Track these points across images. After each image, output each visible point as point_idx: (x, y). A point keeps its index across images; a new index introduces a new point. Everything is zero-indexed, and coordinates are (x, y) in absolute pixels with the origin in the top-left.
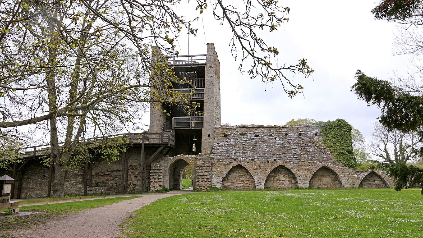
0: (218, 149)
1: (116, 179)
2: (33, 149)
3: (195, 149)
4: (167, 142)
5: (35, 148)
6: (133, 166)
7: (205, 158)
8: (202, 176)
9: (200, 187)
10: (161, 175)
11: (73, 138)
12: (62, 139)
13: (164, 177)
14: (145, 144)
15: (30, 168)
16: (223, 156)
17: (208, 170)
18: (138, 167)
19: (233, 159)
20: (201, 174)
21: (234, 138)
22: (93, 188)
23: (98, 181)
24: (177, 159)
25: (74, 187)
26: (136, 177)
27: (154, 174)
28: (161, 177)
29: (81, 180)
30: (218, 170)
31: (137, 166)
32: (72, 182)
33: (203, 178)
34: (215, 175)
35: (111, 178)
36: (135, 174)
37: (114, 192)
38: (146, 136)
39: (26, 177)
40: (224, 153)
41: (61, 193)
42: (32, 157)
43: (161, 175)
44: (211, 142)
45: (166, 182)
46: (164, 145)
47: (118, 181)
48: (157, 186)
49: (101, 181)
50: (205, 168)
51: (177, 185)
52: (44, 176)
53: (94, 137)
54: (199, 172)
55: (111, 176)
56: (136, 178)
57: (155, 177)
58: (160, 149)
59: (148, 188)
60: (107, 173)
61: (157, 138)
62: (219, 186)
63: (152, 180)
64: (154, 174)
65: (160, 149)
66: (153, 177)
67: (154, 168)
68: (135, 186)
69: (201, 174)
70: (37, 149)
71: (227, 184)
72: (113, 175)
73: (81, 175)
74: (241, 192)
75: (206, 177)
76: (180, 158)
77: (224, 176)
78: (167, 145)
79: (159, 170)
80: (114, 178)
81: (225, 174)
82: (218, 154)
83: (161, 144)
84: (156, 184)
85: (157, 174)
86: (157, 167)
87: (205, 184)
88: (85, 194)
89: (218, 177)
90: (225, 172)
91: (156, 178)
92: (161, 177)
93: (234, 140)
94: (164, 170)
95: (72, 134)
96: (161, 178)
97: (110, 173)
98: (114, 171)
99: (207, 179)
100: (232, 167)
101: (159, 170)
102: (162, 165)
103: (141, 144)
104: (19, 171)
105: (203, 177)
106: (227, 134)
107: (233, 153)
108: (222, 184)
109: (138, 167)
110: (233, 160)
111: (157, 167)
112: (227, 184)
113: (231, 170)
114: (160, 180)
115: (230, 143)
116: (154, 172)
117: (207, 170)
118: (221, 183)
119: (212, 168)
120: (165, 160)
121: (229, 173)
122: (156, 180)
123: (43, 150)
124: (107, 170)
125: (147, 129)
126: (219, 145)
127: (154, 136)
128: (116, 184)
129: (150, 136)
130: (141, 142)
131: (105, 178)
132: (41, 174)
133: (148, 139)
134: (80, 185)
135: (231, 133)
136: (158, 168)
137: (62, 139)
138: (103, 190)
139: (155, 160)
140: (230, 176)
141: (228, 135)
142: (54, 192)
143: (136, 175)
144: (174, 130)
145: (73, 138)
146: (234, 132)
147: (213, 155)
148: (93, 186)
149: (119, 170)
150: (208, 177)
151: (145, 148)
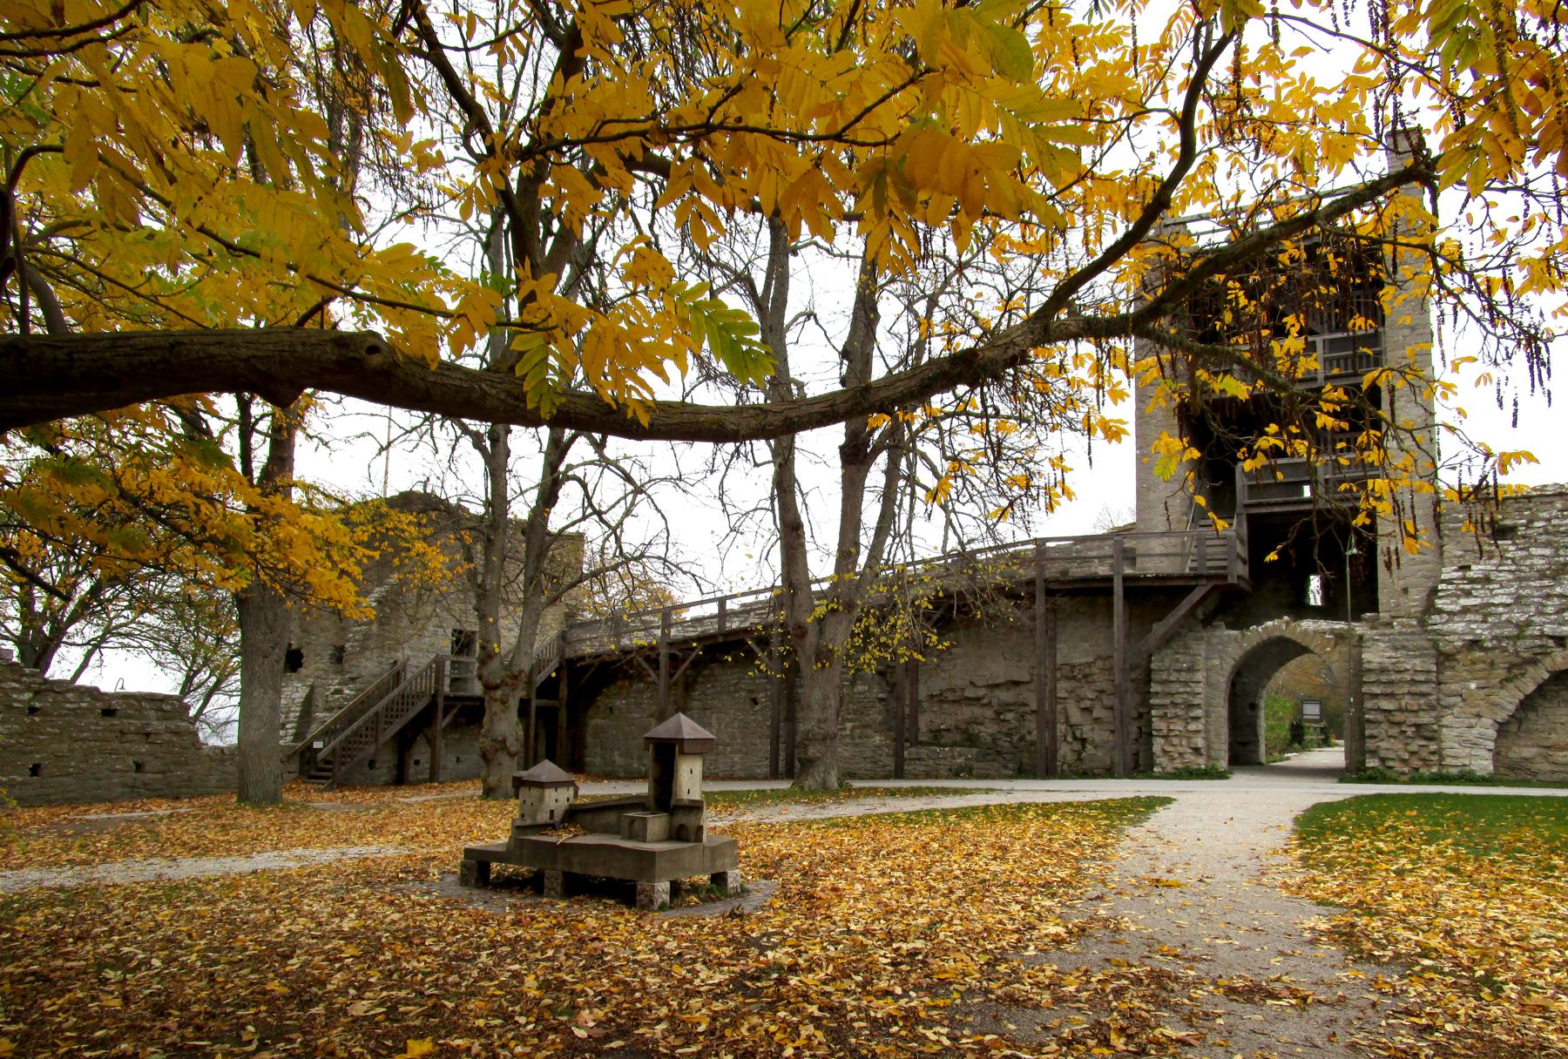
0: (1468, 594)
1: (1010, 716)
2: (713, 609)
3: (1318, 597)
4: (1225, 568)
5: (722, 602)
6: (1073, 667)
7: (1400, 633)
8: (1389, 711)
9: (1383, 760)
10: (1198, 706)
11: (862, 559)
12: (821, 564)
13: (1207, 714)
14: (1126, 579)
15: (706, 672)
16: (1494, 625)
17: (1424, 688)
18: (1095, 670)
19: (1551, 637)
20: (1386, 704)
21: (1547, 545)
22: (923, 751)
23: (938, 721)
24: (1265, 637)
25: (856, 745)
26: (1088, 710)
27: (1167, 701)
28: (1199, 712)
29: (880, 718)
30: (1473, 686)
31: (1089, 665)
32: (849, 725)
33: (1399, 724)
34: (1456, 710)
35: (989, 713)
36: (1080, 699)
37: (1005, 767)
38: (1128, 544)
39: (696, 703)
40: (1501, 609)
41: (827, 772)
42: (712, 636)
43: (1198, 706)
44: (1425, 562)
45: (1218, 735)
46: (1209, 577)
47: (1014, 723)
48: (1181, 749)
49: (950, 722)
50: (1408, 677)
51: (1244, 744)
52: (755, 702)
53: (944, 550)
54: (1375, 696)
55: (989, 704)
56: (1086, 715)
57: (1171, 712)
58: (1195, 596)
59: (1141, 755)
60: (970, 693)
61: (1173, 550)
62: (1483, 763)
63: (1158, 724)
64: (1167, 701)
65: (1195, 596)
66: (1161, 712)
67: (1164, 676)
68: (1084, 747)
69: (1386, 704)
70: (731, 605)
71: (1523, 750)
72: (995, 701)
73: (881, 700)
74: (126, 641)
75: (1412, 719)
76: (1278, 634)
77: (1502, 716)
78: (1225, 577)
79: (1186, 683)
80: (998, 713)
81: (1512, 708)
82: (1469, 617)
83: (1197, 577)
84: (1175, 741)
85: (1178, 699)
86: (1178, 671)
87: (1410, 748)
88: (899, 774)
89: (1473, 721)
90: (1509, 699)
91: (1177, 716)
92: (1199, 712)
93: (1547, 552)
94: (1209, 684)
95: (857, 545)
96: (1196, 718)
97: (981, 692)
98: (997, 686)
99: (1417, 726)
100: (1546, 676)
101: (1186, 683)
102: (1201, 664)
103: (1109, 579)
104: (675, 684)
105: (1399, 717)
106: (1508, 522)
107: (1550, 610)
108: (1497, 755)
109: (1095, 670)
110: (1551, 643)
111: (1178, 671)
112: (1523, 750)
113: (1541, 690)
114: (1192, 727)
115: (1528, 562)
116: (1167, 689)
117: (1414, 689)
118: (1491, 745)
119: (1442, 678)
120: (1209, 643)
121: (1527, 704)
122: (1178, 726)
123: (746, 610)
124: (972, 683)
125: (1125, 514)
126: (1470, 574)
127: (1156, 546)
128: (1007, 735)
129: (1139, 546)
130: (1102, 570)
131: (967, 712)
132: (743, 694)
133: (1130, 557)
134: (878, 739)
135: (1531, 521)
136: (1183, 676)
137: (821, 564)
138: (961, 756)
139: (1167, 641)
140: (1532, 716)
141: (1513, 529)
142: (803, 765)
143: (1088, 703)
144: (1244, 518)
145: (862, 559)
146: (1545, 515)
147: (1436, 618)
148: (922, 743)
149: (1016, 683)
150: (1425, 718)
151: (1128, 593)
